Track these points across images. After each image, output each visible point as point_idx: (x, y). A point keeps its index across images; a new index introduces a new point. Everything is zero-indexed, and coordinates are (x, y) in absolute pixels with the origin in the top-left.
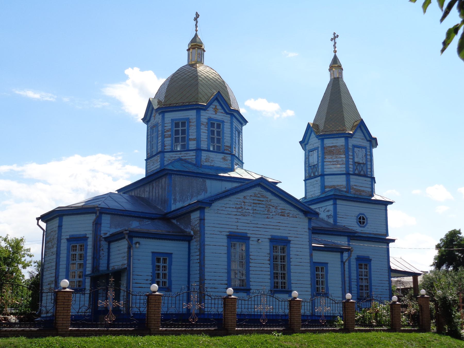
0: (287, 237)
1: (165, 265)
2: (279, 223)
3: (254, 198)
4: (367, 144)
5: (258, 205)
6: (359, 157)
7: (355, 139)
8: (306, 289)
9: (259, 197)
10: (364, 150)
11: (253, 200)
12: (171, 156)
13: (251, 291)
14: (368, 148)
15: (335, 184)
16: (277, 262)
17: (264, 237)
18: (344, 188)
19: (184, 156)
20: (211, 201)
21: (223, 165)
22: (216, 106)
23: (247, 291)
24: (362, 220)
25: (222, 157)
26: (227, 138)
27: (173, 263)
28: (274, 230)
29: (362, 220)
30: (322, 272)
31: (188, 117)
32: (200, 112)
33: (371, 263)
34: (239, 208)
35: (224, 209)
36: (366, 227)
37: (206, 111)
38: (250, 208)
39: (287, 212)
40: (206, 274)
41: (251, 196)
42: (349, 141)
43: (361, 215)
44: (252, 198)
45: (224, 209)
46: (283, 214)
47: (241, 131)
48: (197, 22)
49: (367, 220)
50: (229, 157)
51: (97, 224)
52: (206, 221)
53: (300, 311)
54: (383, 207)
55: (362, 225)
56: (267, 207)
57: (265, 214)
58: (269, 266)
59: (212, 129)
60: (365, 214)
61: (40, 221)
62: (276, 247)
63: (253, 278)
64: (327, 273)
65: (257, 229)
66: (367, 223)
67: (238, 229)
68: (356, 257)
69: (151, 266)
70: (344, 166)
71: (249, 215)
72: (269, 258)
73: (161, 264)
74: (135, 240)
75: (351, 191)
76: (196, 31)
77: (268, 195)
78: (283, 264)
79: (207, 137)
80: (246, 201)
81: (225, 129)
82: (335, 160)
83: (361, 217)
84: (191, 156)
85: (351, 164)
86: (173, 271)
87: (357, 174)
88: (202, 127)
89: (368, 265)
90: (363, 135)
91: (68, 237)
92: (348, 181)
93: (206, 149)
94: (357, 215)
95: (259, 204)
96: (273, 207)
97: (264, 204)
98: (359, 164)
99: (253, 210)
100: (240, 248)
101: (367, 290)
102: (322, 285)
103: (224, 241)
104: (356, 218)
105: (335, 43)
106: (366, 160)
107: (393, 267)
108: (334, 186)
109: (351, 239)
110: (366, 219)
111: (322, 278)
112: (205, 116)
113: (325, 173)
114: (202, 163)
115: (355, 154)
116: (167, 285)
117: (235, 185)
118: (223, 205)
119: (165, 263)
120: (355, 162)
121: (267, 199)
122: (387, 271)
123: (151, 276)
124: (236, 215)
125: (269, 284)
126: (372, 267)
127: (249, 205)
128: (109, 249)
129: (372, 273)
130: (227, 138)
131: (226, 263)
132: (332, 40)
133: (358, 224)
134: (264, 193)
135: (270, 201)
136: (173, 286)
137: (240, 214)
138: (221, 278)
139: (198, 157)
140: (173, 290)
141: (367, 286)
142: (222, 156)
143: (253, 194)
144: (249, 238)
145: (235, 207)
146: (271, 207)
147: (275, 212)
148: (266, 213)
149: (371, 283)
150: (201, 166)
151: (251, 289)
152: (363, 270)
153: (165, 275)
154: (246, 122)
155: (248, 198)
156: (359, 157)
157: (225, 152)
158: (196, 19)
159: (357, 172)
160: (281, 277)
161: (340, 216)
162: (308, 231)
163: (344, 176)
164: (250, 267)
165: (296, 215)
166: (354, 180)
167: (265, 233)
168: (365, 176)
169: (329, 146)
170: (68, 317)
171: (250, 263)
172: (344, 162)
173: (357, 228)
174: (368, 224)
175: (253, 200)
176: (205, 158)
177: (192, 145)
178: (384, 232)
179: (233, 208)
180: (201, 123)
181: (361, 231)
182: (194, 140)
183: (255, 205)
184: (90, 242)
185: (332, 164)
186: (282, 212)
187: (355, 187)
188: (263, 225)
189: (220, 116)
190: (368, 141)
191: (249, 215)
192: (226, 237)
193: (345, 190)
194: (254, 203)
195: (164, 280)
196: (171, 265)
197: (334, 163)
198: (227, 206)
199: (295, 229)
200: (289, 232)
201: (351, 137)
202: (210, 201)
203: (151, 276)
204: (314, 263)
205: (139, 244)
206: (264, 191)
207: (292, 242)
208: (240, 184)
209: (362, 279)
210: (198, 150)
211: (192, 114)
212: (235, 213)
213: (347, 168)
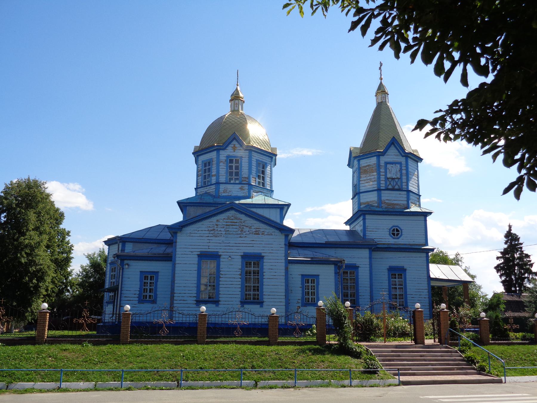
0: (261, 253)
2: (253, 241)
3: (227, 221)
5: (231, 227)
7: (388, 156)
8: (281, 300)
9: (232, 219)
10: (398, 166)
11: (226, 222)
12: (201, 191)
13: (220, 303)
15: (369, 200)
17: (236, 254)
18: (376, 203)
20: (181, 226)
21: (241, 194)
22: (234, 145)
23: (216, 302)
25: (240, 187)
26: (245, 171)
27: (159, 280)
28: (246, 248)
31: (212, 157)
32: (219, 152)
33: (406, 273)
34: (212, 230)
35: (196, 232)
36: (401, 238)
37: (225, 151)
38: (223, 229)
39: (262, 230)
40: (176, 288)
41: (224, 219)
42: (381, 159)
43: (394, 228)
44: (225, 220)
45: (196, 232)
48: (381, 71)
50: (246, 187)
52: (177, 244)
54: (422, 218)
55: (396, 237)
57: (238, 234)
58: (240, 280)
59: (230, 164)
60: (399, 226)
63: (222, 290)
64: (318, 284)
65: (229, 248)
66: (402, 235)
67: (209, 249)
68: (388, 268)
69: (139, 283)
70: (376, 183)
71: (221, 236)
72: (240, 273)
73: (149, 281)
74: (126, 262)
75: (382, 205)
77: (243, 217)
79: (225, 172)
80: (218, 223)
81: (243, 163)
82: (369, 178)
85: (382, 180)
86: (158, 286)
87: (391, 189)
88: (221, 164)
89: (403, 274)
90: (397, 151)
92: (379, 197)
93: (225, 182)
94: (390, 228)
95: (232, 225)
96: (247, 227)
97: (237, 225)
98: (393, 179)
99: (226, 231)
100: (209, 266)
101: (403, 299)
103: (195, 259)
104: (388, 230)
106: (401, 175)
107: (432, 276)
108: (368, 202)
110: (400, 231)
113: (361, 191)
114: (220, 194)
115: (388, 170)
117: (207, 209)
118: (196, 229)
120: (388, 178)
121: (240, 220)
122: (426, 280)
123: (139, 291)
124: (208, 236)
125: (239, 296)
126: (407, 277)
127: (222, 227)
129: (407, 282)
130: (245, 171)
131: (196, 279)
133: (391, 236)
134: (237, 215)
135: (244, 222)
136: (158, 299)
138: (190, 292)
139: (217, 189)
140: (158, 302)
142: (240, 186)
143: (227, 217)
144: (263, 257)
146: (245, 227)
147: (248, 231)
148: (239, 232)
149: (406, 292)
150: (219, 197)
151: (220, 301)
152: (397, 280)
154: (421, 160)
155: (221, 221)
157: (243, 183)
158: (380, 68)
159: (390, 187)
162: (284, 246)
163: (376, 192)
164: (220, 281)
165: (272, 233)
166: (387, 196)
167: (238, 251)
168: (400, 190)
169: (364, 166)
170: (205, 328)
171: (220, 277)
172: (376, 179)
173: (391, 241)
174: (403, 236)
175: (226, 222)
176: (223, 189)
178: (423, 241)
179: (206, 230)
180: (220, 161)
181: (395, 242)
182: (214, 175)
183: (228, 227)
185: (366, 182)
186: (256, 231)
187: (387, 201)
188: (236, 243)
190: (403, 156)
191: (221, 236)
192: (197, 256)
193: (376, 205)
196: (157, 281)
197: (368, 181)
198: (200, 229)
200: (263, 248)
201: (383, 155)
202: (179, 226)
203: (139, 291)
204: (171, 260)
205: (128, 266)
206: (239, 214)
207: (265, 258)
210: (218, 183)
211: (213, 155)
212: (207, 235)
213: (379, 184)
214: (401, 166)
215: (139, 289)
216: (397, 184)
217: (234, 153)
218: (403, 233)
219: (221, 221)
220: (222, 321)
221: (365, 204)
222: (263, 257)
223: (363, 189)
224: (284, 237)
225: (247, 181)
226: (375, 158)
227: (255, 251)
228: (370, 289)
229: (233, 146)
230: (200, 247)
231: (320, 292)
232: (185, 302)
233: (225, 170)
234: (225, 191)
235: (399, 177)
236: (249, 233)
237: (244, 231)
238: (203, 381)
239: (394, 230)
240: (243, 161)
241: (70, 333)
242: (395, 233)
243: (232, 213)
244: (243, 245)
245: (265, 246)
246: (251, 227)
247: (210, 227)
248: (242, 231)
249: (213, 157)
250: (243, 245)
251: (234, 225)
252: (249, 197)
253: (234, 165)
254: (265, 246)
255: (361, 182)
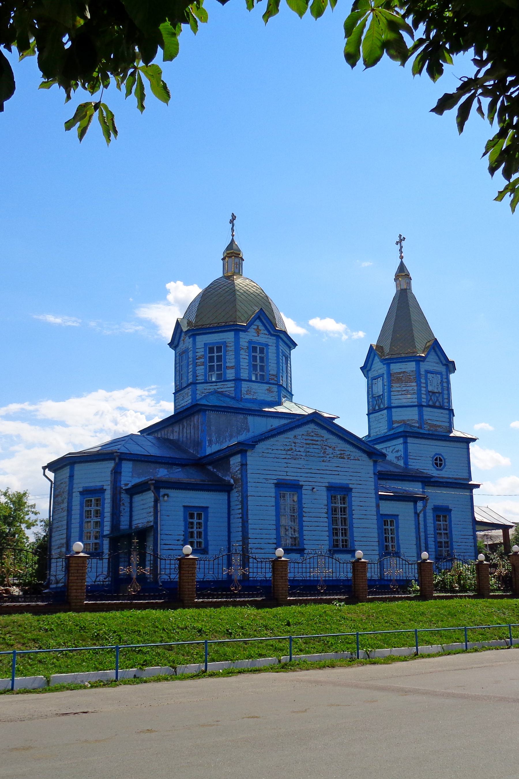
1: (200, 521)
2: (338, 467)
3: (307, 438)
4: (443, 369)
5: (312, 446)
6: (434, 385)
8: (372, 548)
9: (312, 436)
11: (306, 440)
12: (205, 388)
13: (306, 552)
14: (444, 373)
15: (405, 418)
16: (336, 514)
19: (219, 387)
22: (258, 326)
23: (301, 551)
24: (438, 462)
26: (272, 365)
27: (210, 519)
29: (438, 462)
30: (391, 526)
34: (289, 450)
35: (270, 451)
36: (444, 470)
37: (246, 333)
38: (302, 450)
40: (250, 531)
41: (303, 435)
45: (270, 451)
46: (342, 456)
47: (289, 356)
48: (233, 226)
49: (445, 462)
50: (275, 388)
51: (116, 473)
52: (248, 467)
53: (366, 574)
54: (464, 445)
56: (322, 448)
61: (47, 470)
62: (335, 497)
64: (398, 527)
66: (445, 465)
69: (182, 523)
71: (301, 458)
73: (195, 521)
74: (163, 491)
75: (425, 426)
76: (233, 236)
77: (323, 433)
78: (344, 518)
79: (247, 364)
80: (296, 441)
82: (404, 389)
83: (437, 458)
84: (229, 388)
88: (242, 352)
91: (81, 489)
92: (421, 415)
95: (313, 444)
96: (330, 447)
98: (434, 393)
102: (392, 542)
105: (401, 247)
106: (442, 389)
107: (478, 518)
109: (426, 486)
110: (443, 461)
111: (391, 534)
112: (245, 338)
113: (393, 405)
115: (429, 382)
116: (203, 546)
119: (199, 519)
120: (429, 392)
122: (471, 524)
123: (183, 535)
128: (131, 503)
132: (397, 243)
133: (434, 467)
136: (210, 548)
137: (290, 458)
138: (268, 536)
139: (237, 388)
141: (447, 542)
145: (283, 449)
147: (332, 454)
148: (322, 455)
152: (441, 523)
153: (199, 534)
154: (295, 345)
155: (300, 437)
156: (434, 385)
158: (232, 222)
159: (431, 403)
160: (342, 533)
161: (411, 457)
162: (373, 476)
166: (429, 414)
167: (322, 480)
168: (441, 407)
172: (415, 391)
173: (433, 472)
174: (447, 467)
175: (306, 440)
176: (246, 389)
177: (230, 374)
178: (465, 476)
180: (241, 348)
181: (438, 474)
182: (231, 368)
183: (308, 446)
184: (108, 496)
185: (400, 394)
186: (341, 454)
187: (429, 422)
188: (319, 470)
189: (264, 338)
190: (444, 365)
191: (301, 458)
192: (273, 486)
193: (417, 425)
194: (306, 444)
195: (199, 540)
197: (403, 393)
199: (359, 475)
200: (351, 478)
201: (423, 361)
203: (183, 535)
207: (353, 490)
208: (289, 421)
209: (441, 534)
210: (238, 380)
211: (229, 337)
213: (419, 398)
214: (442, 377)
215: (183, 533)
216: (438, 400)
217: (257, 338)
218: (446, 463)
219: (300, 437)
220: (314, 577)
221: (401, 422)
222: (351, 489)
223: (395, 403)
224: (371, 464)
225: (276, 380)
226: (414, 363)
227: (341, 482)
228: (425, 535)
229: (256, 327)
230: (274, 473)
231: (401, 537)
232: (262, 551)
233: (247, 361)
234: (248, 392)
235: (441, 392)
236: (332, 456)
237: (327, 453)
238: (159, 666)
239: (436, 460)
240: (269, 351)
241: (445, 595)
242: (438, 463)
243: (312, 426)
244: (328, 472)
245: (352, 474)
246: (335, 447)
247: (286, 445)
248: (325, 452)
249: (228, 340)
250: (328, 472)
251: (315, 444)
252: (280, 404)
253: (258, 355)
254: (352, 474)
255: (392, 393)
